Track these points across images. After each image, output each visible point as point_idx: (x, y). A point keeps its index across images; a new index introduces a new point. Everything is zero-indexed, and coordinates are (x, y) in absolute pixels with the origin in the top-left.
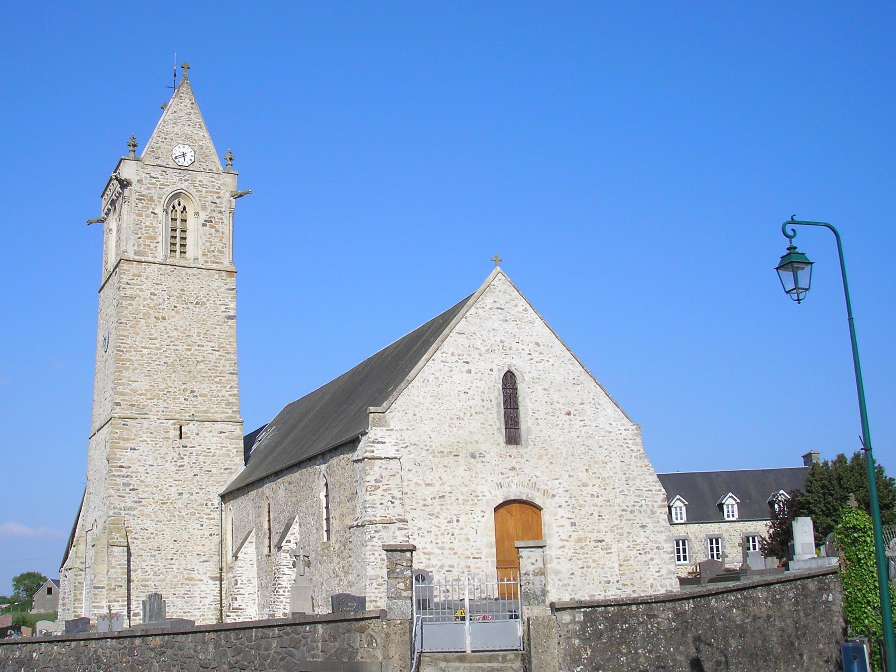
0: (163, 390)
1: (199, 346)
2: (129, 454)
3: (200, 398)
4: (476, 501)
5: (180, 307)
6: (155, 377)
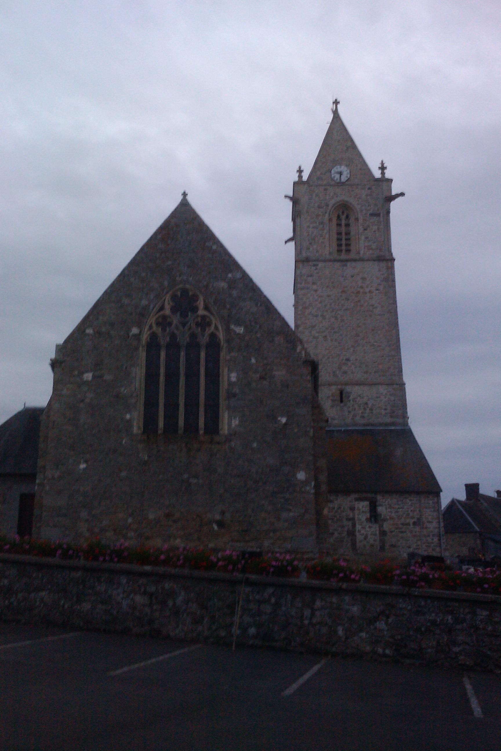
5: (287, 496)
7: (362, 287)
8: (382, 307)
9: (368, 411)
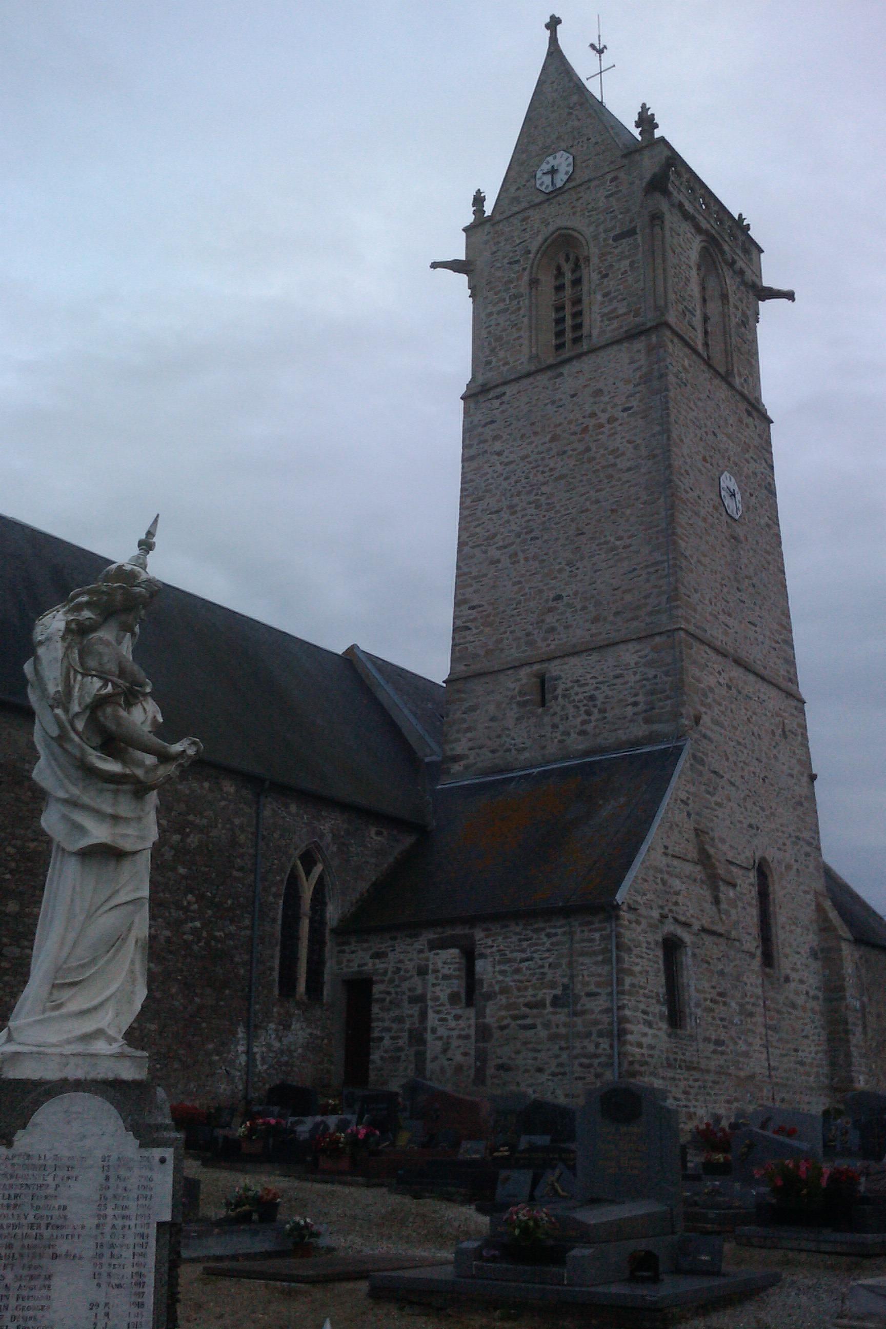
7: (593, 415)
8: (636, 448)
9: (596, 715)
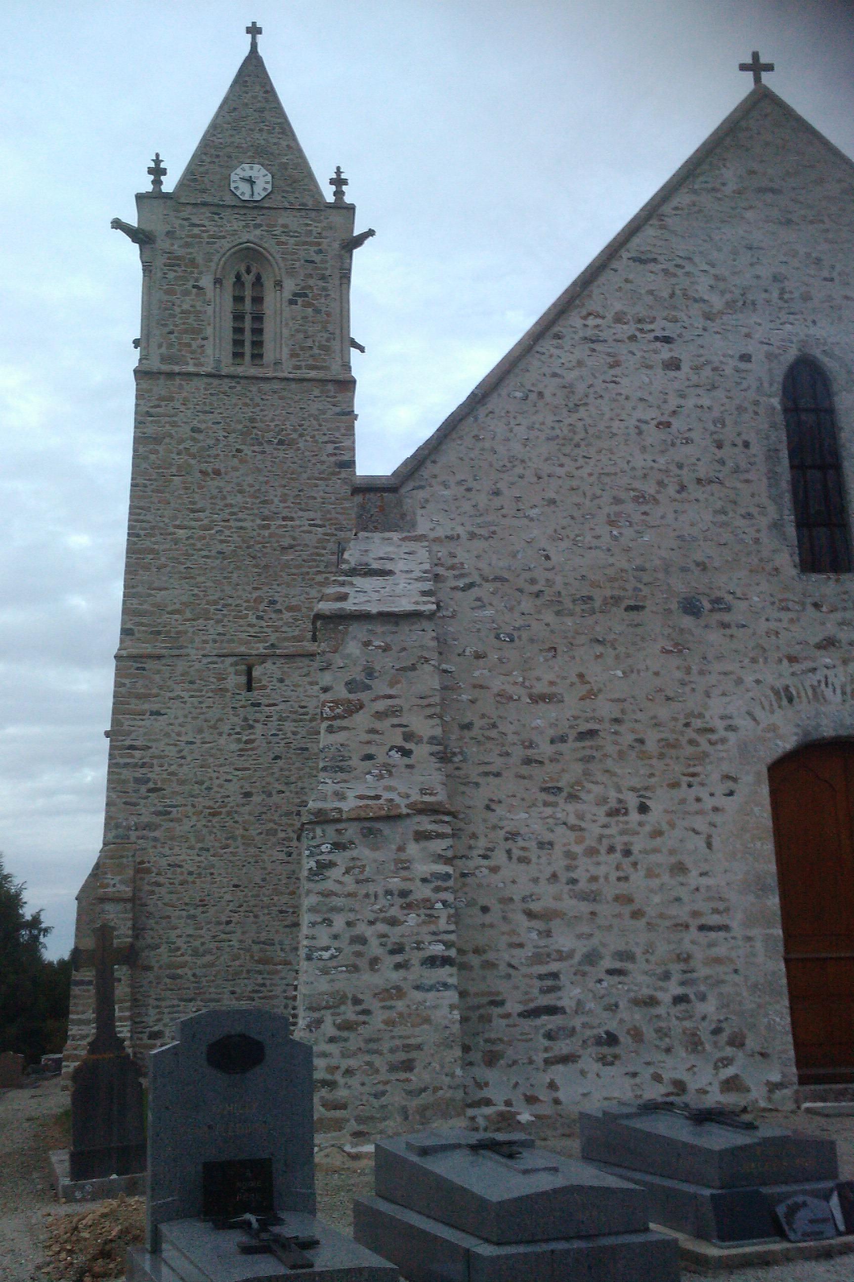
0: (215, 603)
1: (284, 519)
2: (147, 723)
3: (287, 615)
4: (704, 746)
5: (247, 450)
6: (200, 579)
